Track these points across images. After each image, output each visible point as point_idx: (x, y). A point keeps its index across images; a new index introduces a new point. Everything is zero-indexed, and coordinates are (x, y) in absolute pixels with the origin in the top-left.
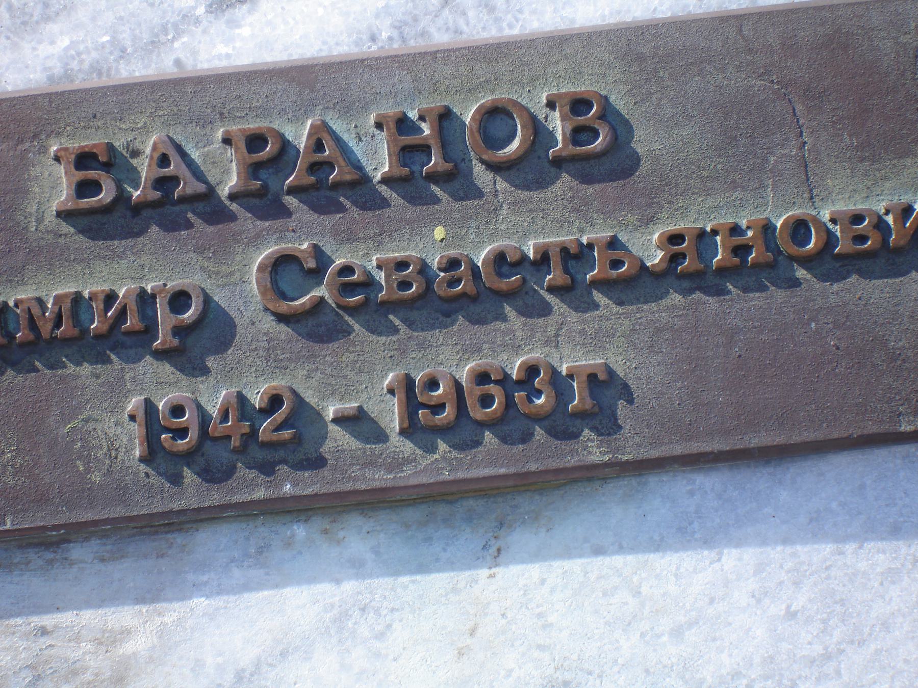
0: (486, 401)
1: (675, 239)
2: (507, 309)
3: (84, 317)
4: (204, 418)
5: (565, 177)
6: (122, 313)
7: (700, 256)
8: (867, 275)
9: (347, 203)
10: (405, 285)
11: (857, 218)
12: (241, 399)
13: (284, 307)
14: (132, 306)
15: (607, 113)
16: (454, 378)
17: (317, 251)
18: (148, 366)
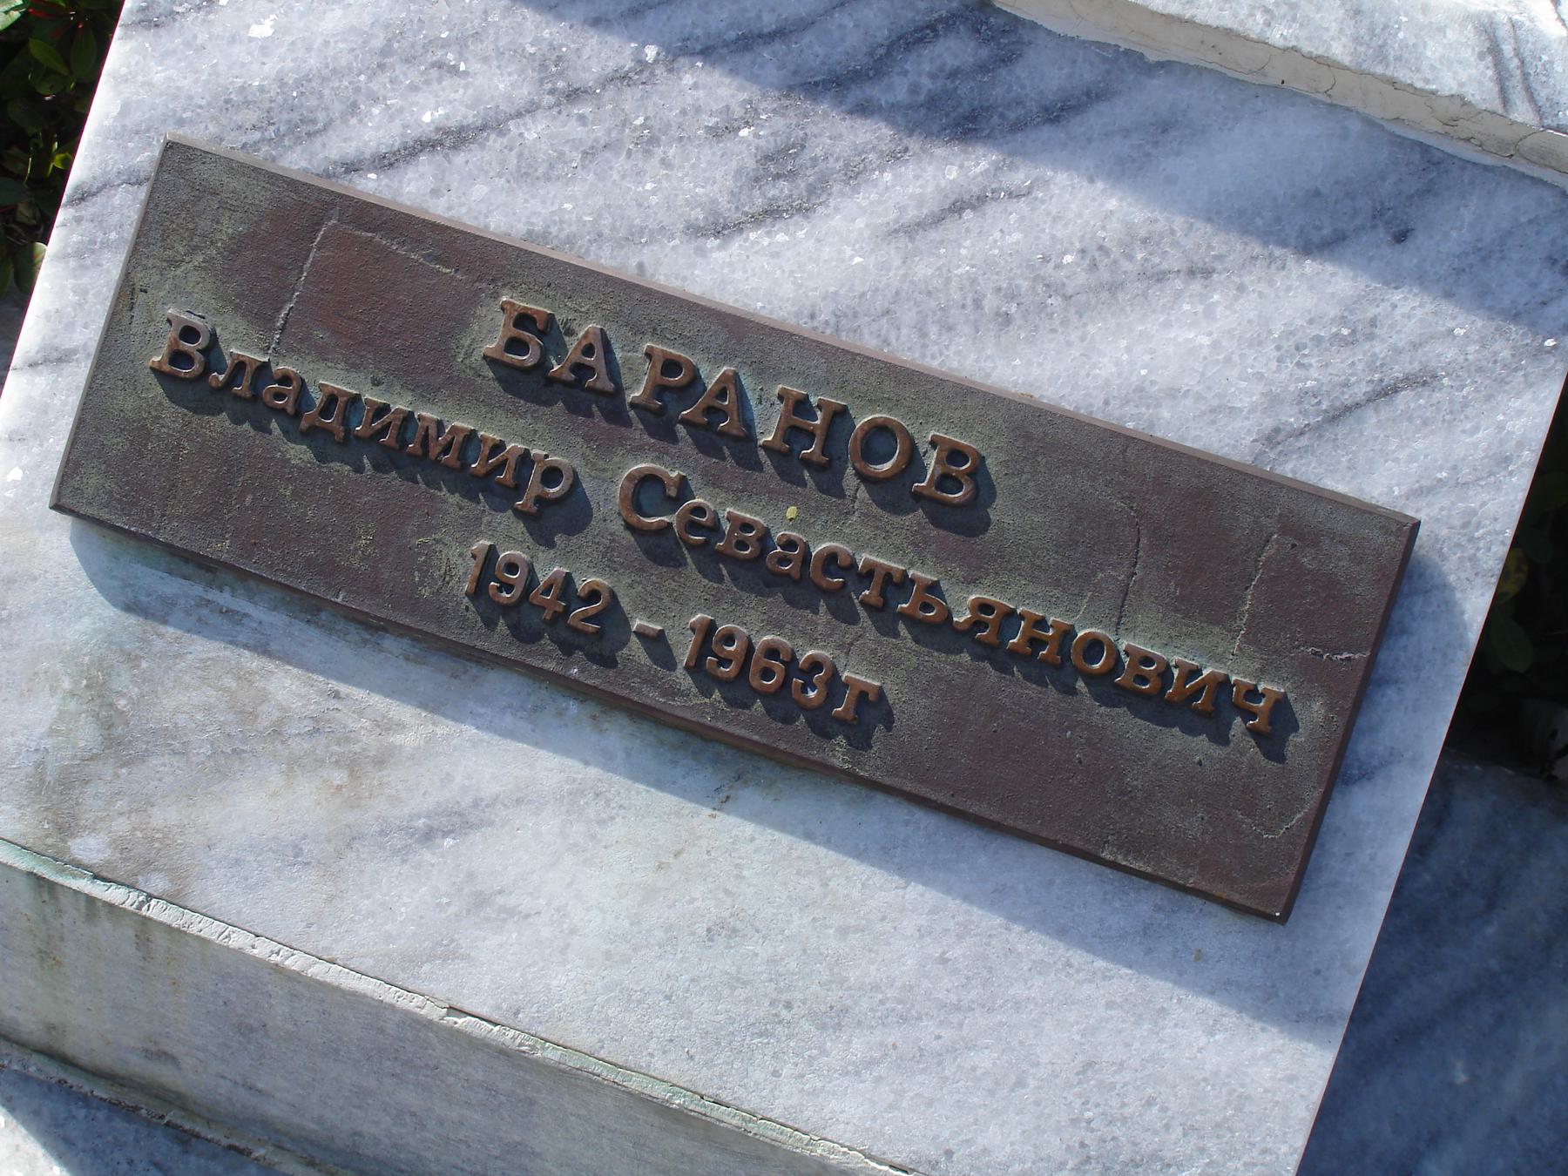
0: (767, 673)
1: (985, 607)
6: (384, 430)
9: (727, 453)
11: (1148, 660)
12: (568, 579)
13: (635, 519)
14: (512, 463)
17: (683, 481)
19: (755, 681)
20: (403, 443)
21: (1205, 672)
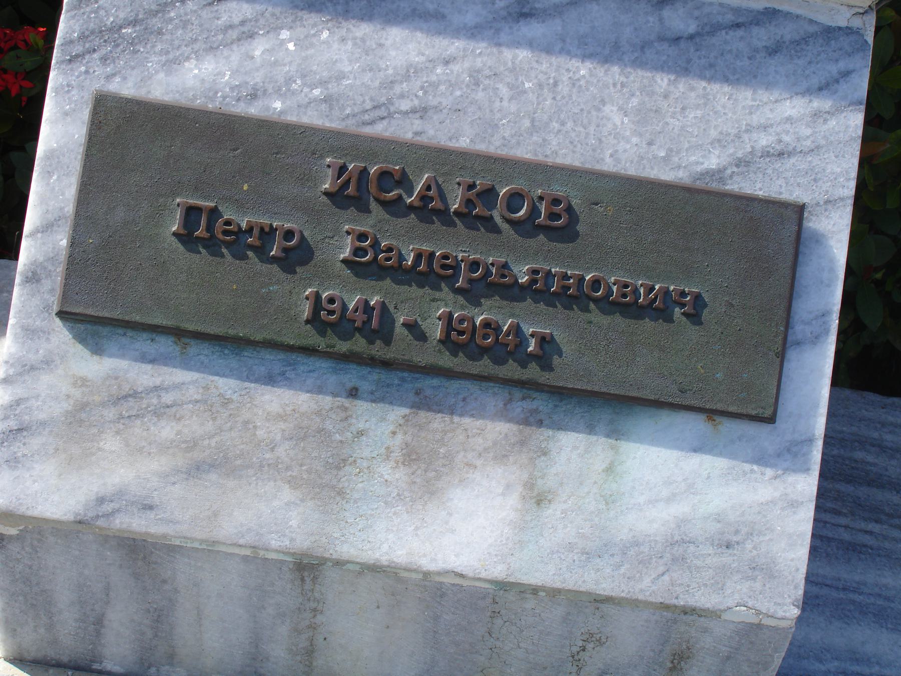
0: (485, 337)
1: (535, 272)
2: (443, 285)
4: (344, 307)
5: (413, 216)
10: (624, 295)
11: (626, 286)
12: (367, 302)
15: (569, 209)
16: (343, 300)
18: (446, 292)
20: (548, 286)
21: (657, 287)
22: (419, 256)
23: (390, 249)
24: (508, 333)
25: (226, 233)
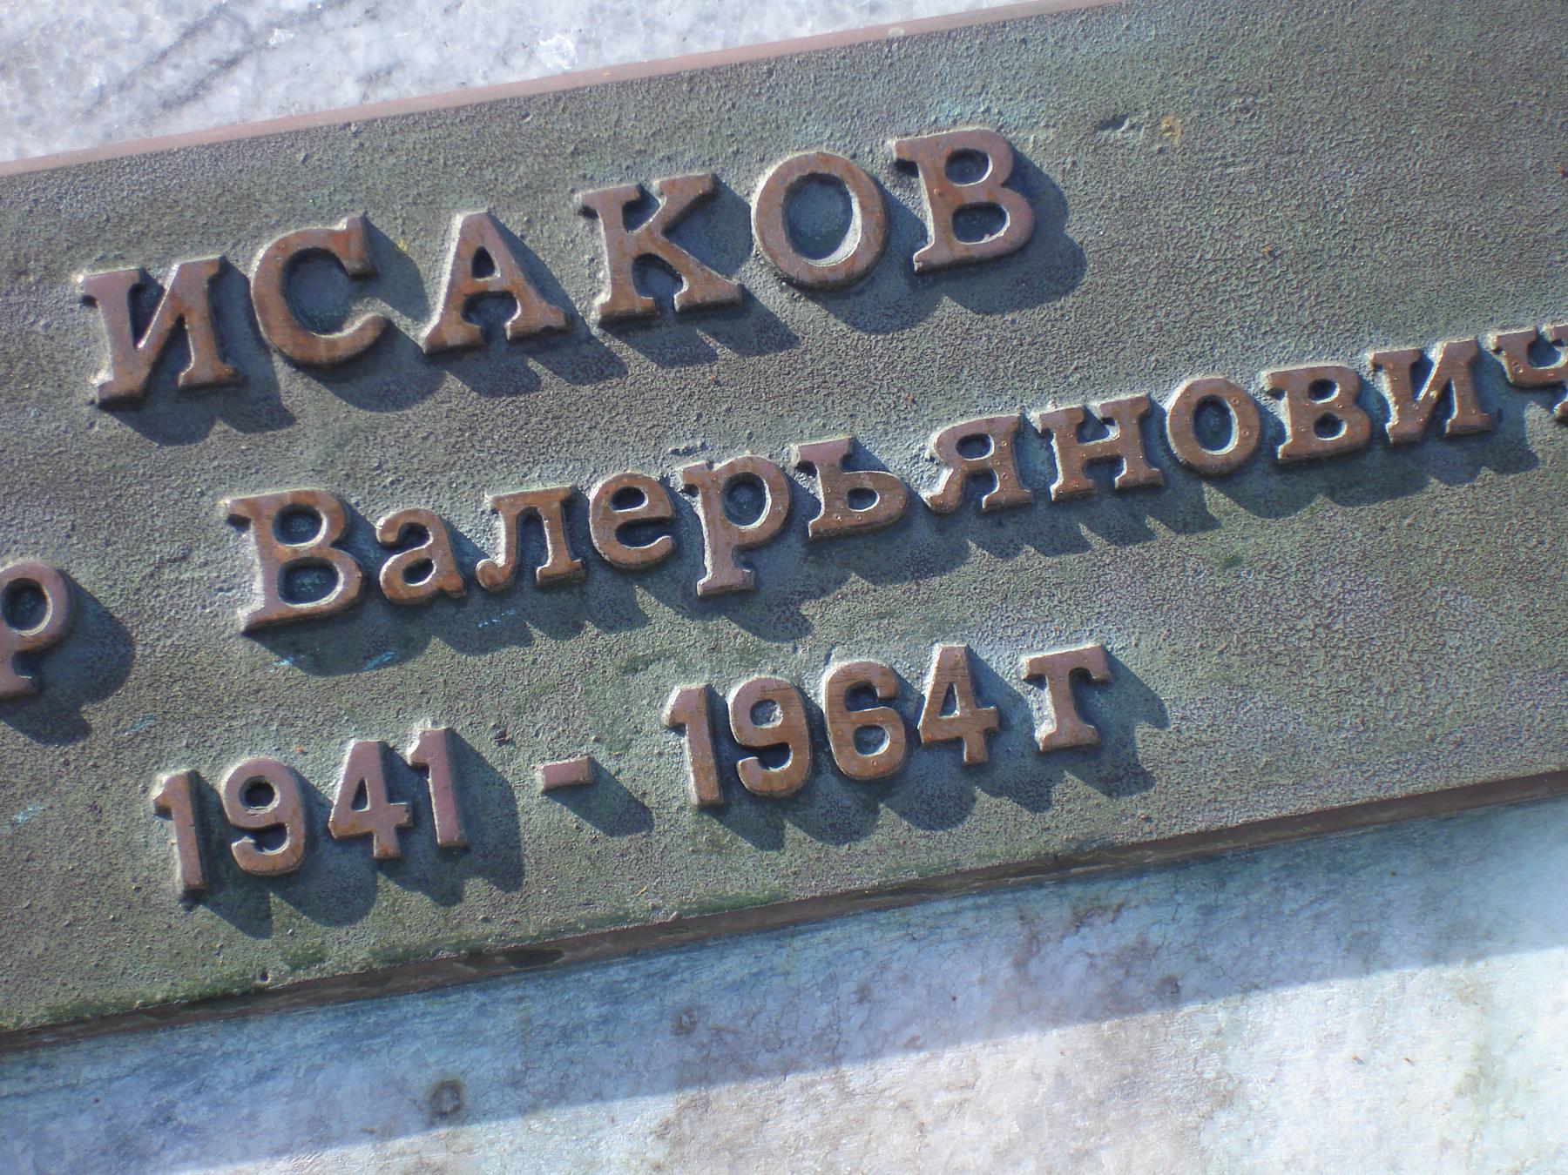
0: (865, 738)
1: (971, 443)
3: (1037, 459)
4: (311, 799)
7: (1024, 476)
8: (1343, 494)
10: (1327, 424)
11: (1321, 387)
12: (388, 754)
15: (1021, 175)
19: (846, 759)
22: (527, 524)
23: (412, 534)
24: (945, 701)
25: (631, 532)
